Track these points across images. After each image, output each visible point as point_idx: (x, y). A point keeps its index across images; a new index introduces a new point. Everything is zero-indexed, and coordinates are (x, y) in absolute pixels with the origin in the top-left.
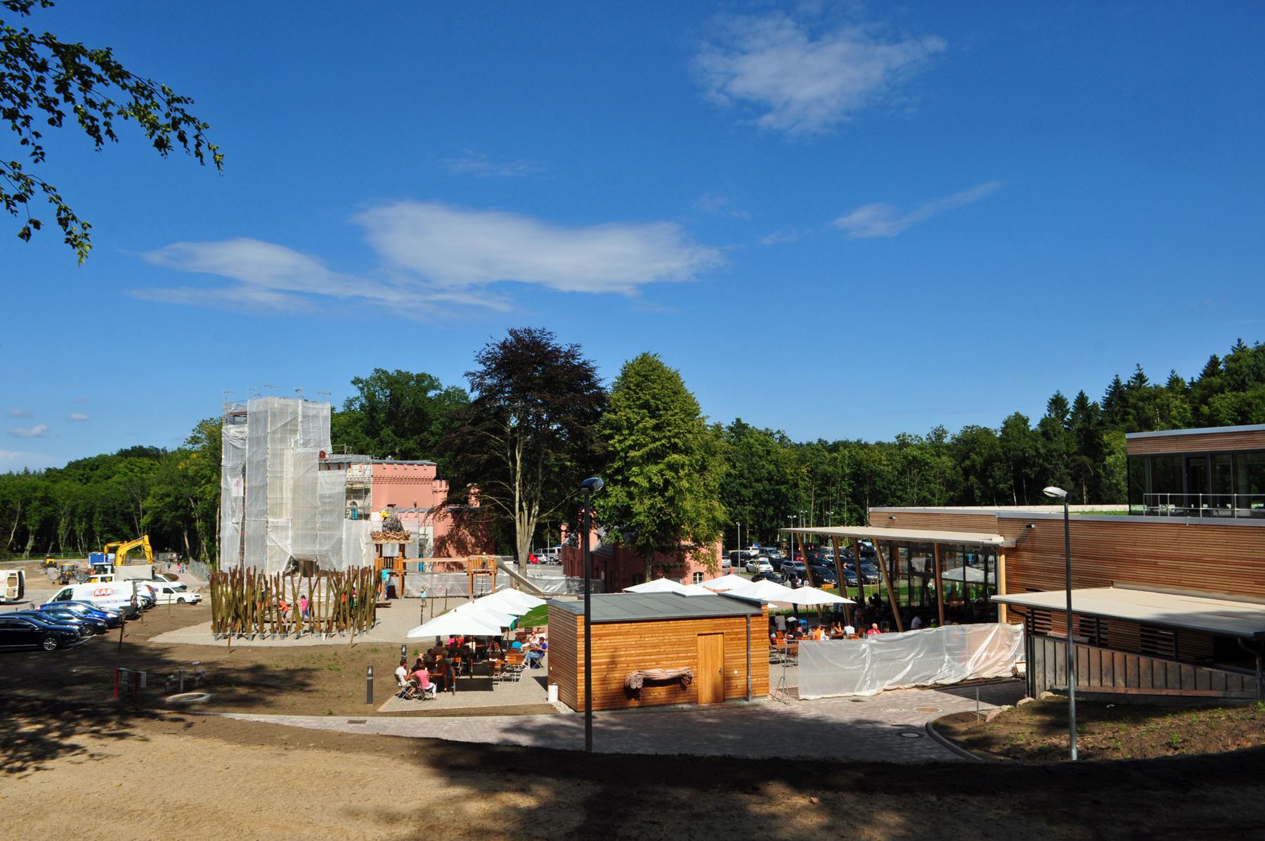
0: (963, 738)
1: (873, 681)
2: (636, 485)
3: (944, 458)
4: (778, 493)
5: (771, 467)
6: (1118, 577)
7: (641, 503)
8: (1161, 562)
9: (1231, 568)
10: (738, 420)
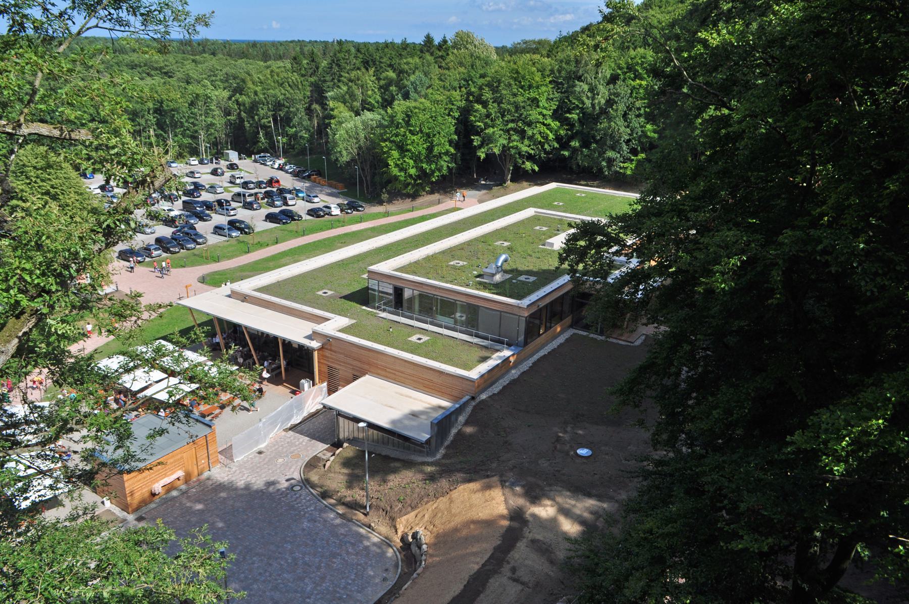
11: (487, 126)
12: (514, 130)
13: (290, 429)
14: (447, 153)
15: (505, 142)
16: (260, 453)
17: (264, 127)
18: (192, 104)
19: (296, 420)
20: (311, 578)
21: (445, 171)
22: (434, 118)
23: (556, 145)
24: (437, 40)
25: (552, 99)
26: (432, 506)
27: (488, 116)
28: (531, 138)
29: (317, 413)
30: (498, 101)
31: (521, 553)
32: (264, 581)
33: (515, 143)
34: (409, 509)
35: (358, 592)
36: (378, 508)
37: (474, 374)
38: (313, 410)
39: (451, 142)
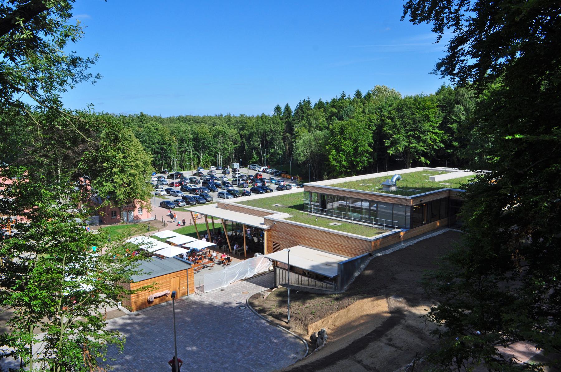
0: (257, 308)
1: (227, 282)
2: (116, 182)
3: (233, 130)
4: (162, 149)
5: (159, 137)
6: (300, 243)
7: (120, 190)
8: (312, 240)
9: (330, 245)
10: (141, 113)
11: (395, 133)
12: (413, 136)
13: (245, 280)
14: (367, 151)
15: (407, 144)
16: (222, 290)
17: (256, 148)
18: (215, 136)
19: (249, 275)
20: (242, 352)
21: (366, 163)
22: (358, 130)
23: (442, 146)
24: (364, 94)
25: (439, 117)
26: (335, 315)
27: (395, 126)
28: (424, 142)
29: (264, 273)
30: (402, 117)
31: (397, 332)
32: (209, 351)
33: (414, 145)
34: (319, 318)
35: (274, 362)
36: (296, 319)
37: (372, 238)
38: (261, 271)
39: (370, 145)
